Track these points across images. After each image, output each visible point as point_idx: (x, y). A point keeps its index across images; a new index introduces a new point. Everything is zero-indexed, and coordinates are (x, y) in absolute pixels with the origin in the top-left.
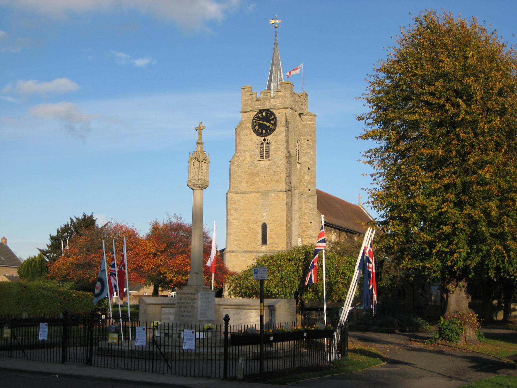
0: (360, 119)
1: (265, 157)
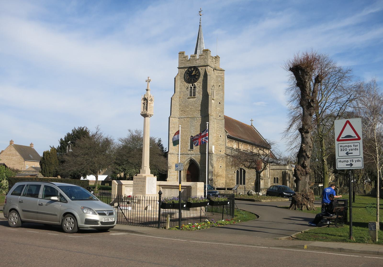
0: (129, 131)
1: (192, 96)
